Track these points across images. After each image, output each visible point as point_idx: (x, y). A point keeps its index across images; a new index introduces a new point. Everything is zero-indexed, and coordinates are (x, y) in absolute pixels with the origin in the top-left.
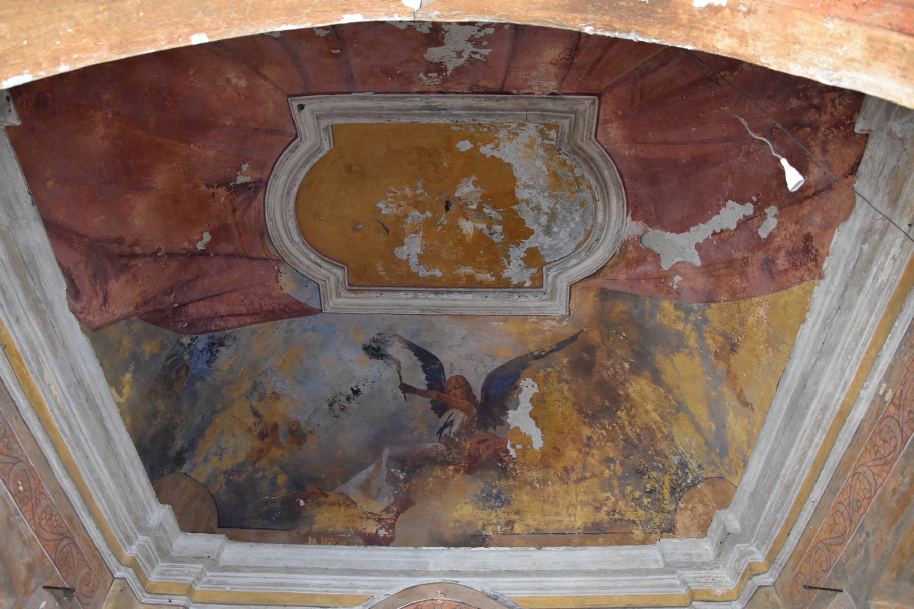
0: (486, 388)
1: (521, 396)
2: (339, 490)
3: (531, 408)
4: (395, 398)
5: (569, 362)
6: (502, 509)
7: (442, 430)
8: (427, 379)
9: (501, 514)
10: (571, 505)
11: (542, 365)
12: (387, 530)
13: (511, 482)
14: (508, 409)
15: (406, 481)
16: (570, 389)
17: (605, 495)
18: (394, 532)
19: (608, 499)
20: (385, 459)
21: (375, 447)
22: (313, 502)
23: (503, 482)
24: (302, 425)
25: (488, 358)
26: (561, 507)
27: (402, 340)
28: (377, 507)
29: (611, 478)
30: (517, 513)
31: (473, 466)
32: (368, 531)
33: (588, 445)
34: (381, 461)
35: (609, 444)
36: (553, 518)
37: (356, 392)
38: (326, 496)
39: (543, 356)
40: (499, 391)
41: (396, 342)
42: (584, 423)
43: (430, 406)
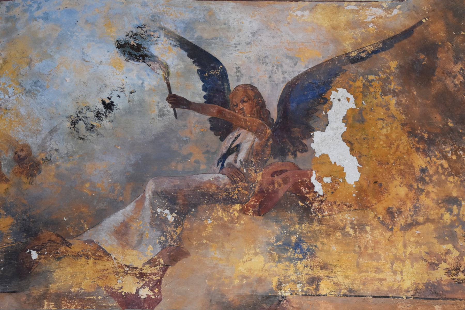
0: (284, 102)
1: (330, 113)
2: (86, 236)
3: (344, 129)
4: (162, 114)
5: (399, 67)
6: (304, 262)
7: (224, 157)
8: (204, 89)
9: (302, 269)
10: (396, 258)
11: (361, 70)
12: (152, 289)
13: (316, 226)
14: (313, 130)
15: (177, 224)
16: (398, 104)
17: (445, 247)
18: (160, 292)
19: (448, 252)
20: (148, 194)
21: (134, 182)
22: (49, 253)
23: (305, 227)
24: (34, 149)
25: (288, 61)
26: (383, 262)
27: (169, 34)
28: (137, 259)
29: (452, 225)
30: (324, 267)
31: (265, 205)
32: (125, 290)
33: (421, 180)
34: (144, 197)
35: (451, 179)
36: (372, 275)
37: (109, 106)
38: (69, 245)
39: (363, 59)
40: (303, 104)
41: (163, 38)
42: (418, 149)
43: (209, 125)
